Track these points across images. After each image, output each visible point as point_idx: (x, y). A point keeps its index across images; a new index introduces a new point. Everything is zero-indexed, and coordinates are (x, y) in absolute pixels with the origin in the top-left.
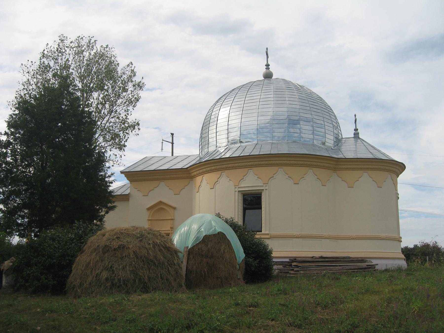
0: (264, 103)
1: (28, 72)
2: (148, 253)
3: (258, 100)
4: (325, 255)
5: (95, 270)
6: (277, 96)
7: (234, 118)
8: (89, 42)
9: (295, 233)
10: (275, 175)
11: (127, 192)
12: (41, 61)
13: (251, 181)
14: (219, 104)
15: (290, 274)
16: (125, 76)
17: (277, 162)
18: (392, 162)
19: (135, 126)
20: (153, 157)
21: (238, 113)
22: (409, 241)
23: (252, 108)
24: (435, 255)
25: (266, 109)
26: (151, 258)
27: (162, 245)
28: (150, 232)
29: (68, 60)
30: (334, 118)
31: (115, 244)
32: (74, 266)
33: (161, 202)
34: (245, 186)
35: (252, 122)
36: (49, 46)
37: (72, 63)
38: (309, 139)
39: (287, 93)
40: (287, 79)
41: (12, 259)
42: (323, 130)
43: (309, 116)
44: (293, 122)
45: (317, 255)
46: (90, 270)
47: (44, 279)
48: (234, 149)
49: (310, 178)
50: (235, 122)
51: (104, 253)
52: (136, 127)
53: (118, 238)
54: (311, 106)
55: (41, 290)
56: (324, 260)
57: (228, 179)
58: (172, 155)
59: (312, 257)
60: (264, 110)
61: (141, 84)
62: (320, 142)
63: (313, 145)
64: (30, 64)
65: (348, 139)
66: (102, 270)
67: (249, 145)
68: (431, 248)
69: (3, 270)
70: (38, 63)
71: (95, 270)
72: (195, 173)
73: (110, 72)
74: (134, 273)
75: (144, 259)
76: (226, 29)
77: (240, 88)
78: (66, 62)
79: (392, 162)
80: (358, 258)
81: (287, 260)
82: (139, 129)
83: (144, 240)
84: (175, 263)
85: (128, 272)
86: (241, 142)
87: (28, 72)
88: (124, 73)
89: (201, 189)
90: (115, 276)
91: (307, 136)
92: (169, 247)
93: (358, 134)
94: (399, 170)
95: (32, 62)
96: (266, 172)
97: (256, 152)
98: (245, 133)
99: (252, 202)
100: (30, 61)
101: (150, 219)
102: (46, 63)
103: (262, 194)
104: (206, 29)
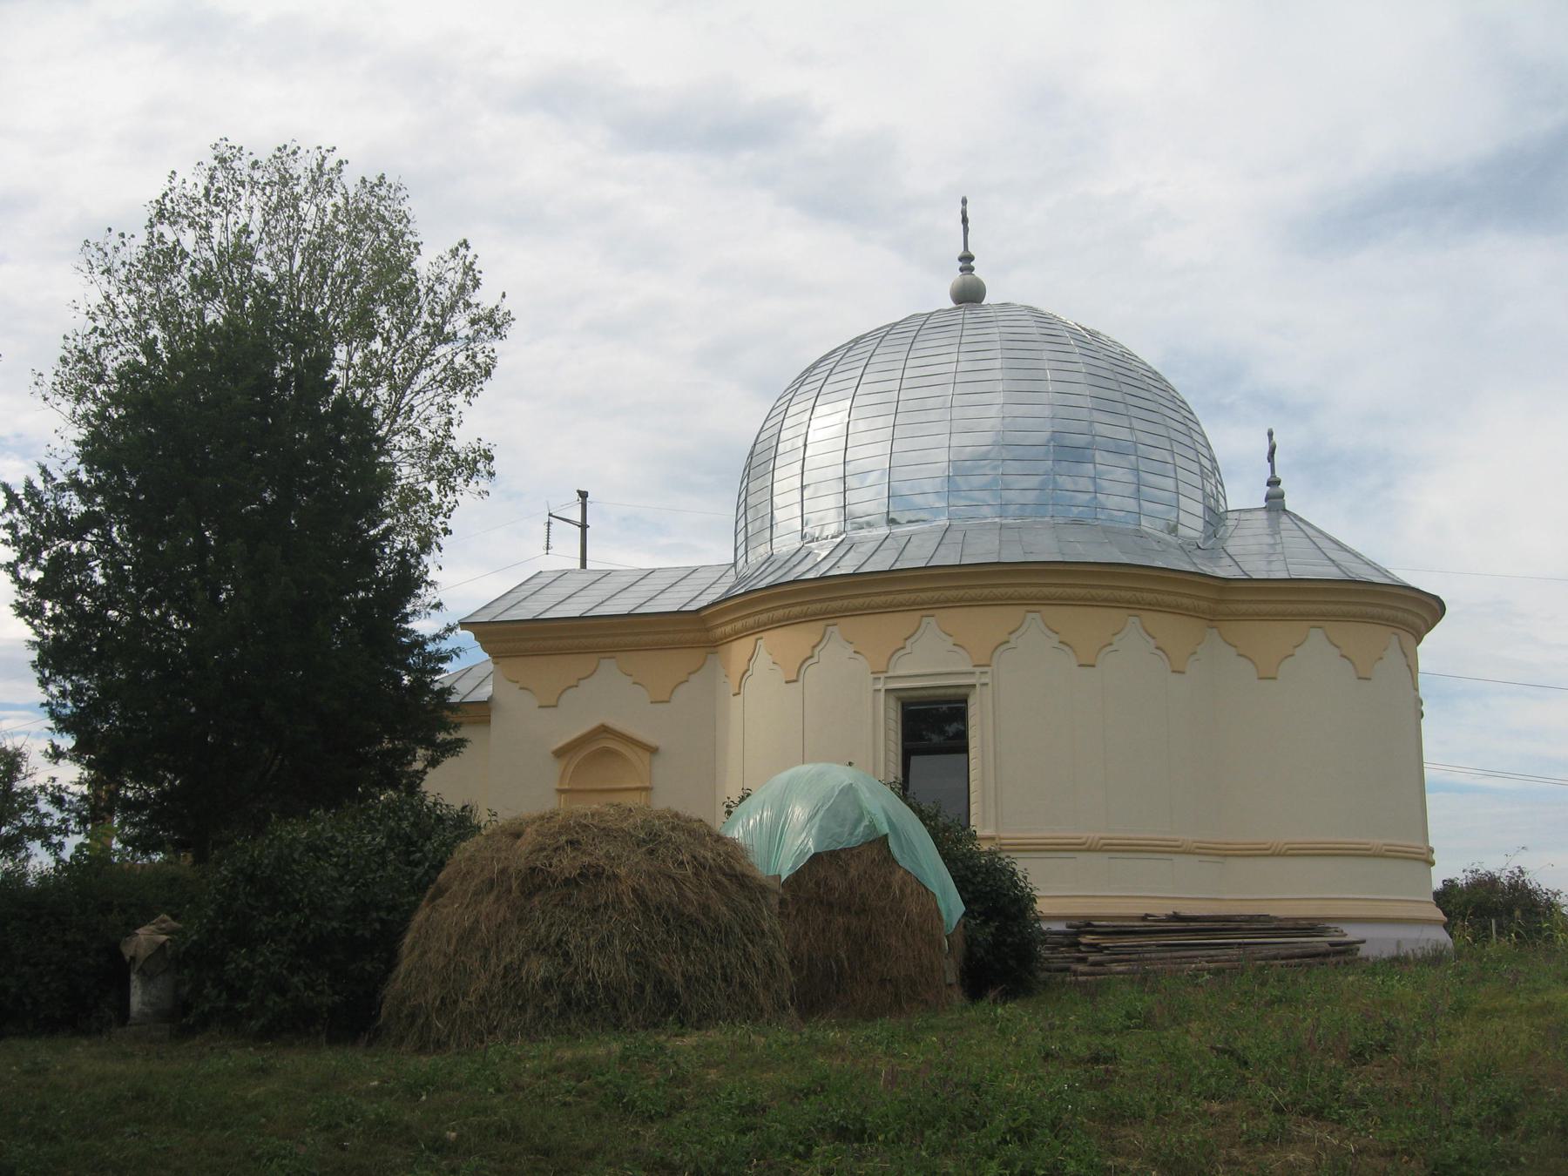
0: (971, 388)
1: (108, 271)
2: (682, 895)
3: (950, 378)
5: (498, 954)
6: (1016, 364)
7: (866, 438)
8: (320, 167)
11: (484, 693)
12: (151, 233)
13: (931, 656)
14: (809, 389)
15: (1075, 973)
16: (444, 292)
17: (1022, 591)
18: (1402, 592)
19: (477, 463)
21: (880, 422)
22: (1452, 864)
23: (930, 403)
24: (1517, 913)
25: (980, 410)
26: (690, 910)
27: (721, 868)
28: (574, 835)
29: (246, 230)
30: (1201, 440)
31: (567, 863)
32: (408, 940)
33: (604, 730)
35: (933, 455)
36: (177, 182)
37: (261, 241)
38: (1133, 514)
41: (164, 921)
42: (1169, 483)
43: (1124, 434)
44: (1068, 451)
46: (477, 955)
47: (301, 986)
48: (868, 548)
49: (1134, 646)
50: (871, 453)
51: (529, 895)
52: (480, 466)
54: (1130, 400)
55: (293, 1025)
56: (1182, 925)
57: (851, 649)
58: (584, 565)
59: (1145, 918)
60: (971, 412)
61: (498, 317)
62: (1160, 524)
63: (1140, 534)
64: (117, 241)
65: (1248, 516)
66: (527, 954)
67: (923, 532)
68: (1503, 892)
69: (133, 958)
70: (142, 238)
71: (498, 954)
72: (728, 629)
73: (390, 275)
75: (670, 916)
76: (727, 132)
77: (883, 334)
78: (238, 236)
79: (1402, 592)
80: (1296, 919)
81: (1060, 927)
82: (491, 474)
83: (662, 850)
84: (766, 927)
85: (618, 957)
87: (108, 271)
88: (440, 279)
89: (750, 684)
91: (1117, 501)
92: (743, 875)
93: (1282, 496)
95: (122, 235)
96: (984, 624)
97: (949, 557)
98: (904, 489)
99: (932, 728)
100: (115, 232)
102: (170, 238)
103: (971, 701)
104: (656, 130)
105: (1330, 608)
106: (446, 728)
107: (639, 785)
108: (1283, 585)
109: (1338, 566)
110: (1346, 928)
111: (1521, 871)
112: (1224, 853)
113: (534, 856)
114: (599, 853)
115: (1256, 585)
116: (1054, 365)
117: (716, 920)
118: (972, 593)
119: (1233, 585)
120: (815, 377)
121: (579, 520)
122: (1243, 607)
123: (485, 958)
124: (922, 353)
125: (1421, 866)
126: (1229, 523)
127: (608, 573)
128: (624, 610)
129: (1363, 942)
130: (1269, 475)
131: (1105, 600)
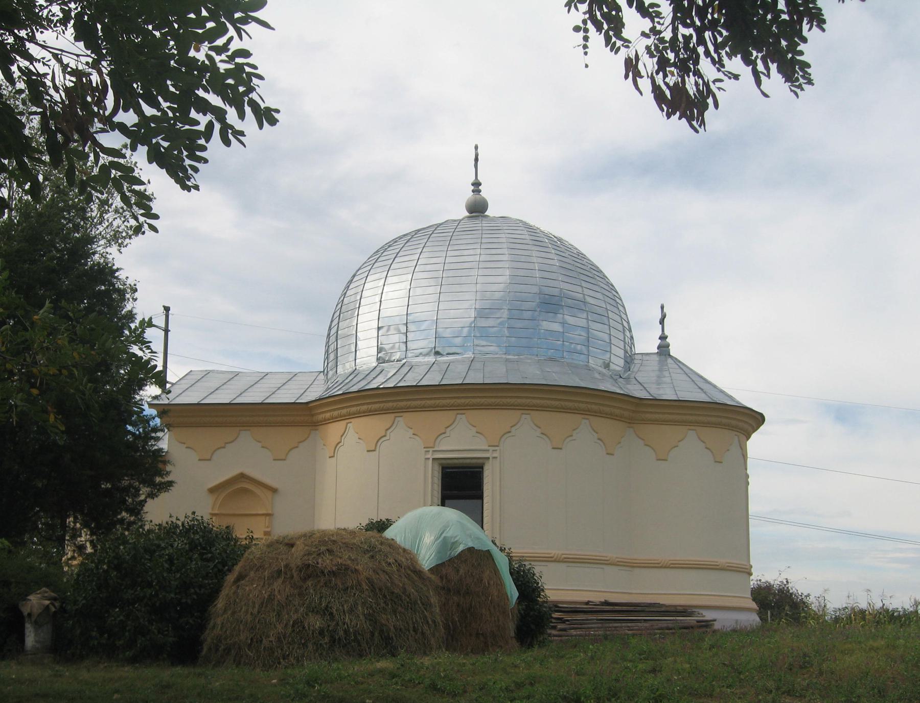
4: (613, 599)
7: (391, 295)
10: (513, 429)
13: (461, 440)
17: (535, 402)
18: (742, 410)
21: (431, 290)
22: (766, 571)
27: (409, 568)
33: (242, 476)
34: (457, 448)
35: (460, 312)
40: (532, 222)
48: (424, 369)
51: (305, 580)
53: (330, 551)
57: (411, 431)
59: (587, 603)
65: (647, 358)
69: (30, 615)
72: (328, 415)
74: (370, 620)
79: (742, 410)
80: (675, 606)
86: (437, 353)
89: (341, 451)
93: (668, 346)
94: (751, 425)
97: (475, 378)
98: (447, 333)
101: (216, 512)
103: (486, 468)
105: (701, 418)
106: (161, 476)
107: (265, 512)
109: (705, 393)
110: (705, 613)
112: (631, 565)
113: (306, 557)
114: (345, 557)
116: (540, 260)
117: (409, 596)
119: (645, 402)
121: (163, 326)
122: (648, 416)
123: (279, 615)
124: (456, 247)
126: (636, 362)
127: (237, 374)
129: (715, 620)
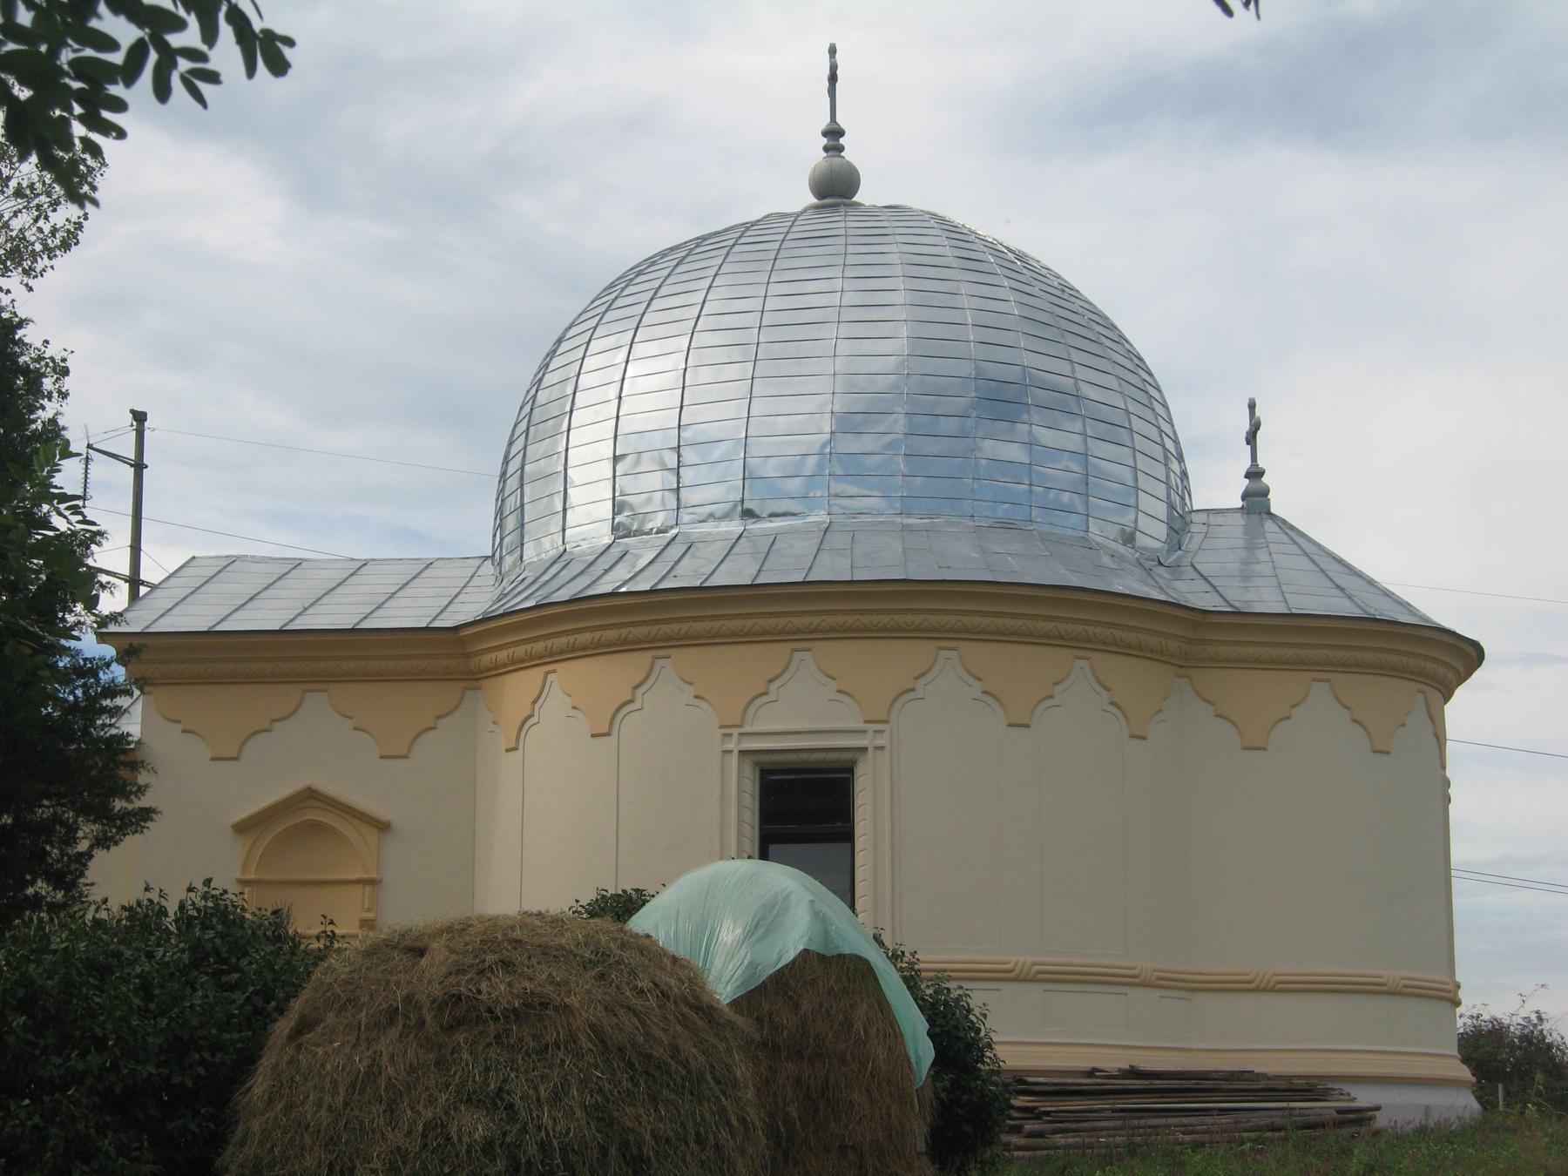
0: (861, 330)
4: (1147, 1062)
9: (1016, 958)
10: (920, 683)
13: (803, 707)
17: (900, 619)
20: (233, 560)
21: (733, 372)
26: (657, 1052)
33: (310, 796)
35: (799, 420)
39: (964, 288)
45: (1113, 1062)
49: (1080, 702)
53: (507, 965)
57: (691, 691)
59: (1091, 1073)
62: (1113, 531)
65: (1219, 519)
72: (502, 655)
74: (599, 1119)
79: (1436, 636)
80: (1289, 1078)
82: (64, 395)
85: (578, 1112)
86: (748, 514)
89: (533, 736)
90: (524, 1130)
93: (1265, 492)
97: (832, 568)
98: (770, 469)
101: (251, 876)
103: (859, 771)
106: (126, 796)
108: (1279, 622)
109: (1349, 597)
110: (1355, 1091)
111: (1540, 1019)
113: (452, 979)
115: (1249, 620)
118: (867, 619)
120: (630, 292)
122: (1225, 651)
123: (391, 1110)
125: (1447, 1005)
126: (1193, 528)
127: (298, 564)
128: (345, 622)
129: (1378, 1108)
130: (1249, 464)
131: (1046, 636)
